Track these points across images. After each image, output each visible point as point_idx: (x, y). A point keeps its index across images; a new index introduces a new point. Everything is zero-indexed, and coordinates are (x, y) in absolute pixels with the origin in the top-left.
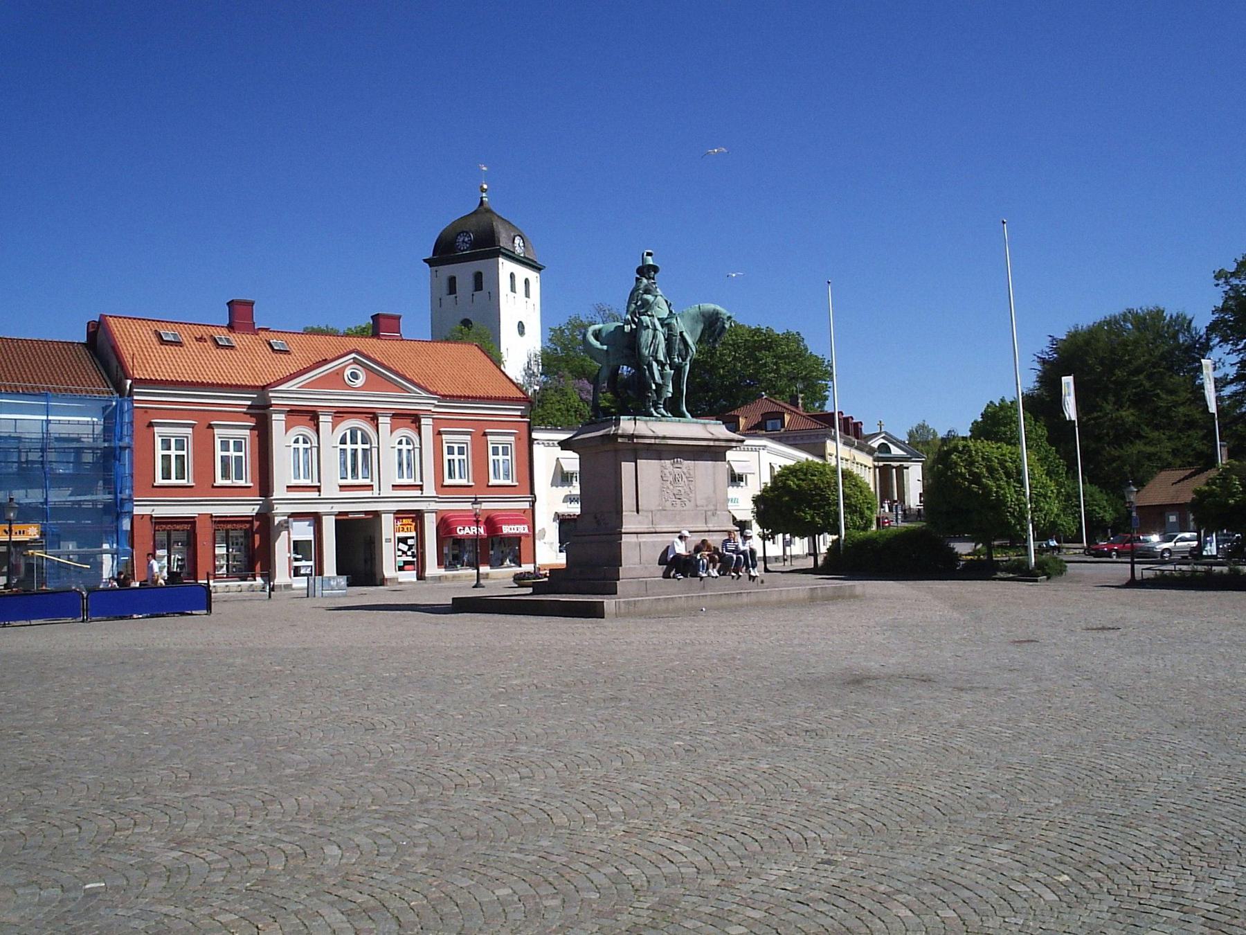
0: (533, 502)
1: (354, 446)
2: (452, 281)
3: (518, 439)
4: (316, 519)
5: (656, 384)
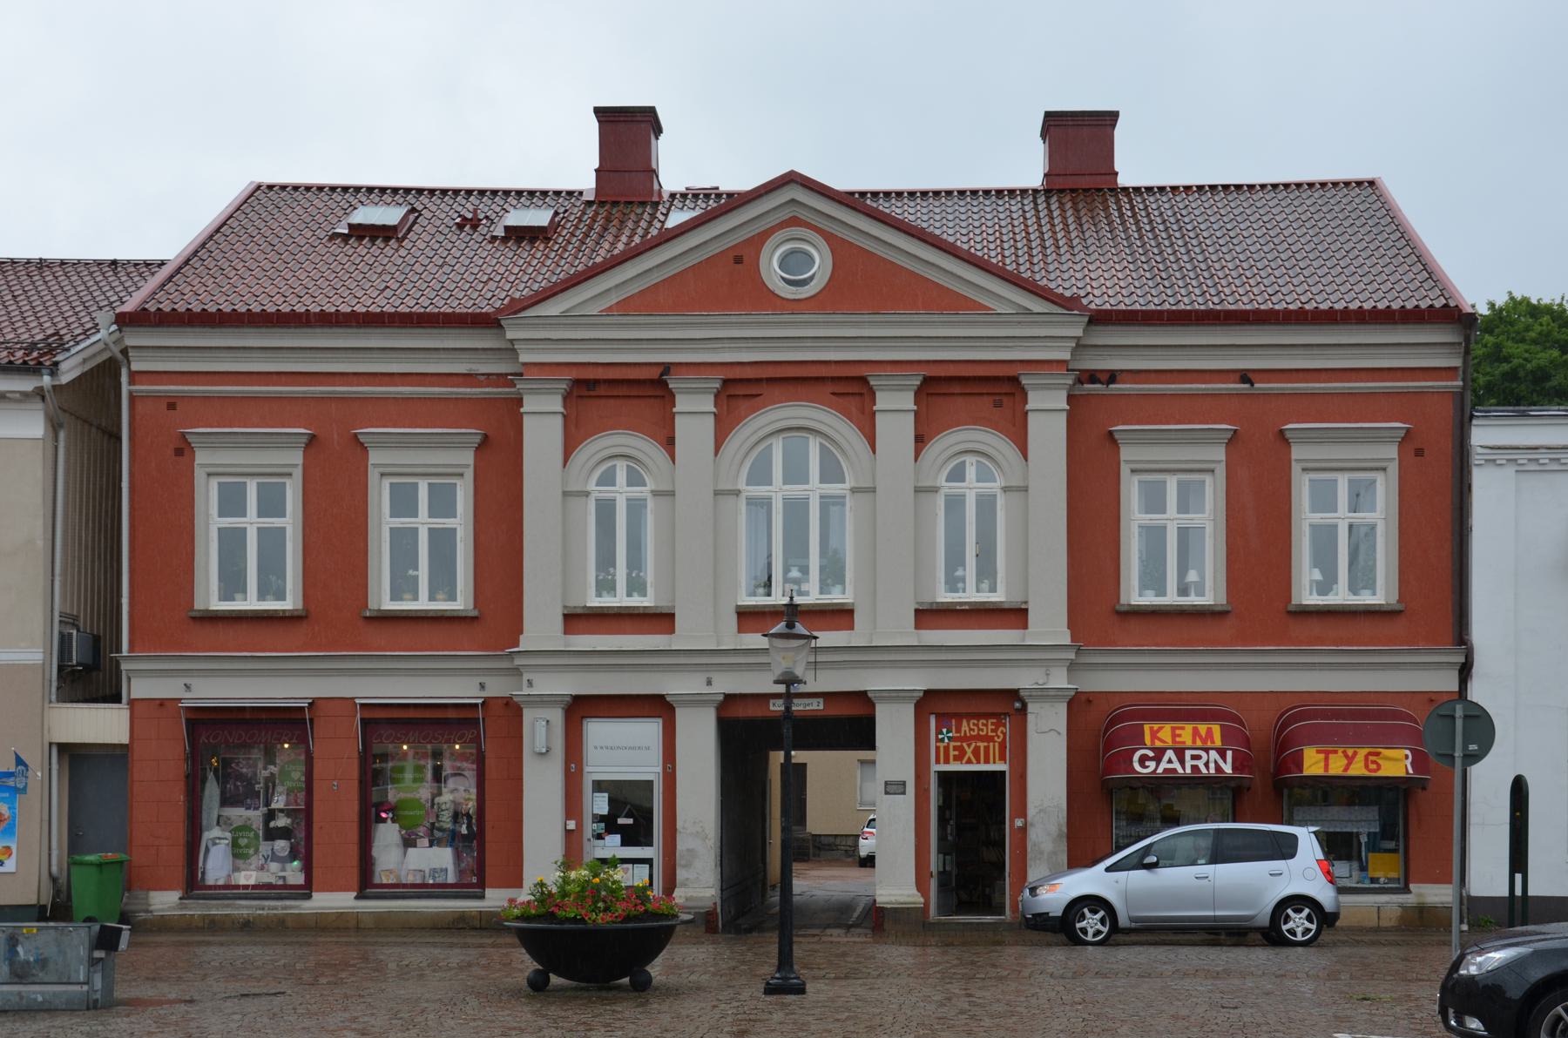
0: (1465, 671)
4: (659, 707)
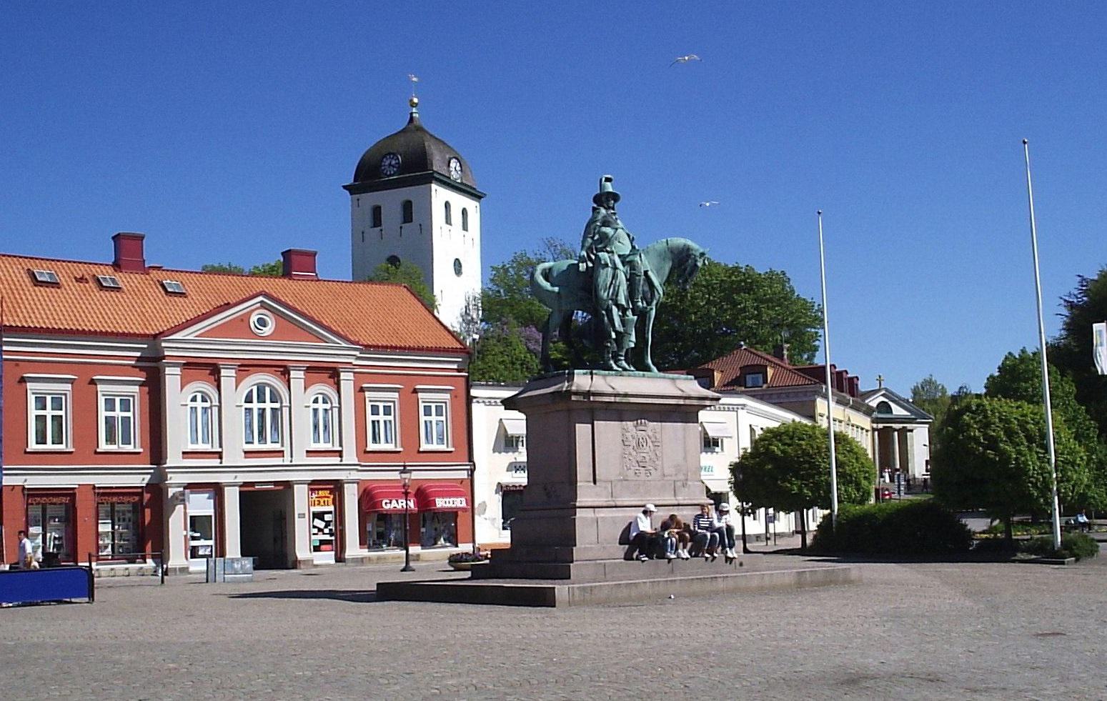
0: (472, 471)
1: (262, 405)
2: (377, 211)
3: (455, 397)
4: (217, 491)
5: (617, 332)
